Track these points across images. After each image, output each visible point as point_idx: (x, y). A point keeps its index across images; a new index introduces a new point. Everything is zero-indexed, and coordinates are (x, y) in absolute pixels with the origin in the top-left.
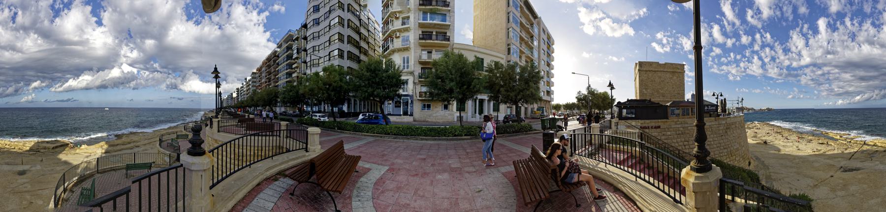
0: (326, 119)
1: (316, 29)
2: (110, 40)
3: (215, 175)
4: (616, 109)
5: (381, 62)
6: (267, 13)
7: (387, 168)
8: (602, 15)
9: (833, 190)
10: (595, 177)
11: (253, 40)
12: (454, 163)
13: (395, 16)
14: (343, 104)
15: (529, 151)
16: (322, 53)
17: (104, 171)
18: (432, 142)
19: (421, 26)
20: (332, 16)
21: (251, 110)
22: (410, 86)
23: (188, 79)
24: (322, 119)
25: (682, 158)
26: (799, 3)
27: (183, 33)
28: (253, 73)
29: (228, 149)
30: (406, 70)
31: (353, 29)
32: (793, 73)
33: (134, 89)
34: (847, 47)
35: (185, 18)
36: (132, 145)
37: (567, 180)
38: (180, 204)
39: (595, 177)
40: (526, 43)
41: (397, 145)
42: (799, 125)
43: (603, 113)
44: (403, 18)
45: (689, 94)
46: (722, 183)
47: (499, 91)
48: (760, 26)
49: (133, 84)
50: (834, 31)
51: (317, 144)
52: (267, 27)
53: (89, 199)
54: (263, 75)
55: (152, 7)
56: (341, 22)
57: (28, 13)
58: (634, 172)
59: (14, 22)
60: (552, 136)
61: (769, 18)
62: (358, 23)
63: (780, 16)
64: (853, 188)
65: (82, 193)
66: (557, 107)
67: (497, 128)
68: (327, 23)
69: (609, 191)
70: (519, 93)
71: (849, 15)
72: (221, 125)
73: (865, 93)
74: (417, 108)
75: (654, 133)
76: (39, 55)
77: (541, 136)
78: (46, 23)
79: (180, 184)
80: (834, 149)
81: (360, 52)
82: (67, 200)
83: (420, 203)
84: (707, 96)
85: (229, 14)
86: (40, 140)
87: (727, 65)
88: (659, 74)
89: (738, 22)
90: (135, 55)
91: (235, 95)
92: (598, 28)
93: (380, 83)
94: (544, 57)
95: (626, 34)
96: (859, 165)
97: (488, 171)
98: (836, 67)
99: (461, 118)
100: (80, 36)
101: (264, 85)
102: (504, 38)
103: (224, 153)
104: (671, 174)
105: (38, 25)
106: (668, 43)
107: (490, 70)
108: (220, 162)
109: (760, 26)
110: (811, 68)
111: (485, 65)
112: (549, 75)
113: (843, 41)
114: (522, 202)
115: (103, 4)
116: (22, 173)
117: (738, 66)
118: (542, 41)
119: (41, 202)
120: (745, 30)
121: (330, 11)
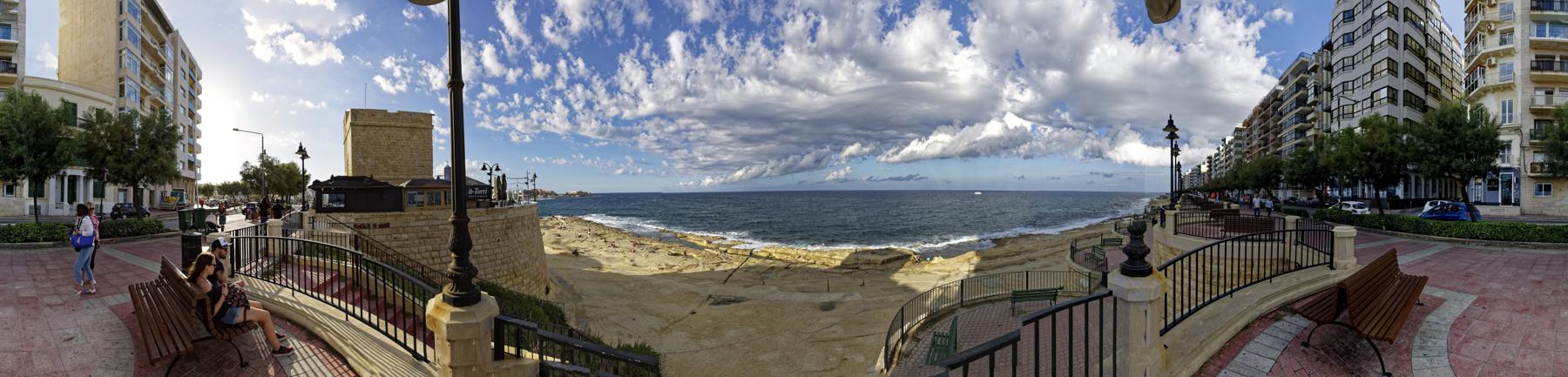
0: (1366, 211)
1: (1349, 51)
2: (983, 71)
3: (1170, 310)
4: (310, 193)
5: (1462, 111)
6: (1261, 24)
7: (1474, 298)
8: (286, 27)
9: (696, 337)
10: (273, 314)
11: (1239, 73)
12: (25, 289)
13: (1487, 28)
14: (1396, 185)
15: (157, 268)
16: (1359, 95)
17: (973, 304)
18: (1553, 252)
19: (1534, 45)
20: (1377, 28)
21: (1233, 194)
22: (1515, 151)
23: (1123, 141)
24: (1359, 211)
25: (428, 281)
26: (635, 6)
27: (1112, 58)
28: (1237, 130)
29: (1193, 265)
30: (1507, 124)
31: (1415, 52)
32: (623, 129)
33: (1026, 157)
34: (720, 82)
35: (1116, 31)
36: (1023, 257)
37: (225, 319)
38: (1108, 362)
39: (273, 314)
40: (153, 76)
41: (1492, 257)
42: (634, 221)
43: (288, 201)
44: (1503, 33)
45: (440, 168)
46: (499, 323)
47: (103, 162)
48: (565, 46)
49: (1023, 149)
50: (697, 55)
51: (1350, 255)
52: (1261, 48)
53: (949, 356)
54: (1255, 132)
55: (1059, 11)
56: (1393, 39)
57: (838, 24)
58: (343, 304)
59: (813, 40)
60: (198, 242)
61: (582, 33)
62: (1423, 44)
63: (601, 28)
64: (730, 334)
65: (934, 343)
66: (208, 190)
67: (101, 228)
68: (1367, 40)
69: (299, 339)
70: (139, 166)
71: (724, 27)
72: (1180, 221)
73: (751, 165)
74: (1527, 192)
75: (379, 236)
76: (858, 98)
77: (178, 242)
78: (871, 40)
79: (1108, 326)
80: (697, 264)
81: (1427, 93)
82: (907, 355)
83: (1532, 360)
84: (472, 170)
85: (1194, 25)
86: (860, 248)
87: (507, 115)
88: (388, 131)
89: (526, 40)
90: (1027, 97)
91: (1204, 169)
92: (279, 50)
93: (1462, 147)
94: (184, 101)
95: (329, 61)
96: (741, 292)
97: (85, 303)
98: (701, 118)
99: (36, 208)
100: (931, 64)
101: (1255, 151)
102: (113, 70)
103: (1186, 272)
104: (409, 309)
105: (857, 45)
106: (404, 77)
107: (89, 125)
108: (1178, 287)
109: (565, 46)
110: (657, 120)
111: (80, 115)
112: (193, 133)
113: (713, 73)
114: (146, 361)
115: (971, 7)
116: (828, 307)
117: (527, 117)
118: (180, 72)
119: (861, 359)
120: (540, 53)
121: (1373, 20)
